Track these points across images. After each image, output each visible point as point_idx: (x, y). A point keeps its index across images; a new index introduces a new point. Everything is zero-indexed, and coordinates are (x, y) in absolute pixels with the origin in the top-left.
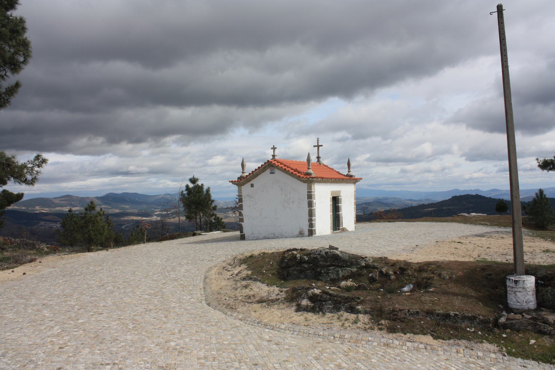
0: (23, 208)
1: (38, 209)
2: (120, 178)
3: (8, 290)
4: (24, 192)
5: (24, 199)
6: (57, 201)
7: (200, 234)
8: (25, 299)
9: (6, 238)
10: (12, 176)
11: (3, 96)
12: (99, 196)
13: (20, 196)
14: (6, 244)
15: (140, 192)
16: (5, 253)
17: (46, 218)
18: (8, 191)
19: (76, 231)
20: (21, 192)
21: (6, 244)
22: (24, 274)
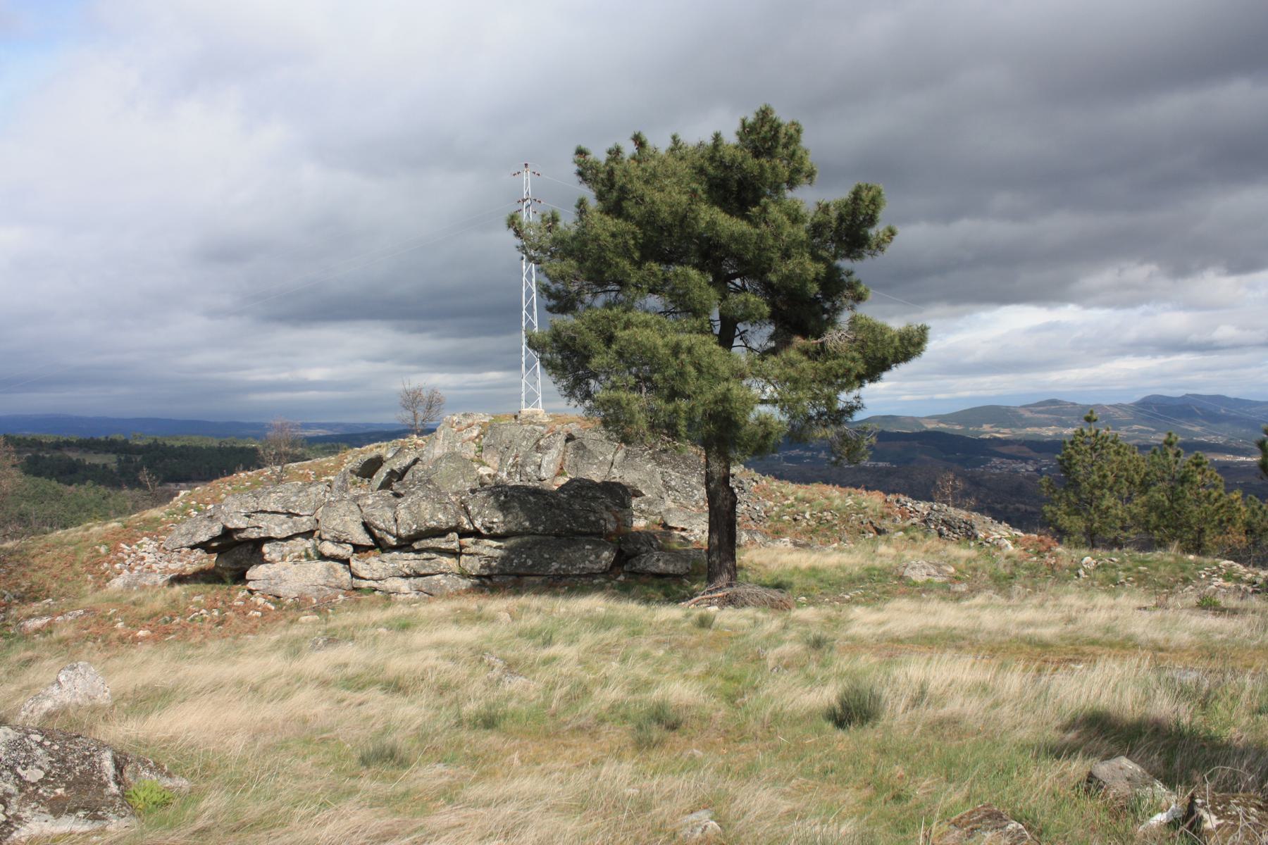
0: (957, 427)
1: (988, 431)
2: (1184, 359)
6: (1028, 414)
9: (891, 497)
12: (1126, 402)
14: (889, 515)
15: (1232, 392)
16: (883, 549)
17: (1004, 450)
19: (1111, 489)
21: (889, 515)
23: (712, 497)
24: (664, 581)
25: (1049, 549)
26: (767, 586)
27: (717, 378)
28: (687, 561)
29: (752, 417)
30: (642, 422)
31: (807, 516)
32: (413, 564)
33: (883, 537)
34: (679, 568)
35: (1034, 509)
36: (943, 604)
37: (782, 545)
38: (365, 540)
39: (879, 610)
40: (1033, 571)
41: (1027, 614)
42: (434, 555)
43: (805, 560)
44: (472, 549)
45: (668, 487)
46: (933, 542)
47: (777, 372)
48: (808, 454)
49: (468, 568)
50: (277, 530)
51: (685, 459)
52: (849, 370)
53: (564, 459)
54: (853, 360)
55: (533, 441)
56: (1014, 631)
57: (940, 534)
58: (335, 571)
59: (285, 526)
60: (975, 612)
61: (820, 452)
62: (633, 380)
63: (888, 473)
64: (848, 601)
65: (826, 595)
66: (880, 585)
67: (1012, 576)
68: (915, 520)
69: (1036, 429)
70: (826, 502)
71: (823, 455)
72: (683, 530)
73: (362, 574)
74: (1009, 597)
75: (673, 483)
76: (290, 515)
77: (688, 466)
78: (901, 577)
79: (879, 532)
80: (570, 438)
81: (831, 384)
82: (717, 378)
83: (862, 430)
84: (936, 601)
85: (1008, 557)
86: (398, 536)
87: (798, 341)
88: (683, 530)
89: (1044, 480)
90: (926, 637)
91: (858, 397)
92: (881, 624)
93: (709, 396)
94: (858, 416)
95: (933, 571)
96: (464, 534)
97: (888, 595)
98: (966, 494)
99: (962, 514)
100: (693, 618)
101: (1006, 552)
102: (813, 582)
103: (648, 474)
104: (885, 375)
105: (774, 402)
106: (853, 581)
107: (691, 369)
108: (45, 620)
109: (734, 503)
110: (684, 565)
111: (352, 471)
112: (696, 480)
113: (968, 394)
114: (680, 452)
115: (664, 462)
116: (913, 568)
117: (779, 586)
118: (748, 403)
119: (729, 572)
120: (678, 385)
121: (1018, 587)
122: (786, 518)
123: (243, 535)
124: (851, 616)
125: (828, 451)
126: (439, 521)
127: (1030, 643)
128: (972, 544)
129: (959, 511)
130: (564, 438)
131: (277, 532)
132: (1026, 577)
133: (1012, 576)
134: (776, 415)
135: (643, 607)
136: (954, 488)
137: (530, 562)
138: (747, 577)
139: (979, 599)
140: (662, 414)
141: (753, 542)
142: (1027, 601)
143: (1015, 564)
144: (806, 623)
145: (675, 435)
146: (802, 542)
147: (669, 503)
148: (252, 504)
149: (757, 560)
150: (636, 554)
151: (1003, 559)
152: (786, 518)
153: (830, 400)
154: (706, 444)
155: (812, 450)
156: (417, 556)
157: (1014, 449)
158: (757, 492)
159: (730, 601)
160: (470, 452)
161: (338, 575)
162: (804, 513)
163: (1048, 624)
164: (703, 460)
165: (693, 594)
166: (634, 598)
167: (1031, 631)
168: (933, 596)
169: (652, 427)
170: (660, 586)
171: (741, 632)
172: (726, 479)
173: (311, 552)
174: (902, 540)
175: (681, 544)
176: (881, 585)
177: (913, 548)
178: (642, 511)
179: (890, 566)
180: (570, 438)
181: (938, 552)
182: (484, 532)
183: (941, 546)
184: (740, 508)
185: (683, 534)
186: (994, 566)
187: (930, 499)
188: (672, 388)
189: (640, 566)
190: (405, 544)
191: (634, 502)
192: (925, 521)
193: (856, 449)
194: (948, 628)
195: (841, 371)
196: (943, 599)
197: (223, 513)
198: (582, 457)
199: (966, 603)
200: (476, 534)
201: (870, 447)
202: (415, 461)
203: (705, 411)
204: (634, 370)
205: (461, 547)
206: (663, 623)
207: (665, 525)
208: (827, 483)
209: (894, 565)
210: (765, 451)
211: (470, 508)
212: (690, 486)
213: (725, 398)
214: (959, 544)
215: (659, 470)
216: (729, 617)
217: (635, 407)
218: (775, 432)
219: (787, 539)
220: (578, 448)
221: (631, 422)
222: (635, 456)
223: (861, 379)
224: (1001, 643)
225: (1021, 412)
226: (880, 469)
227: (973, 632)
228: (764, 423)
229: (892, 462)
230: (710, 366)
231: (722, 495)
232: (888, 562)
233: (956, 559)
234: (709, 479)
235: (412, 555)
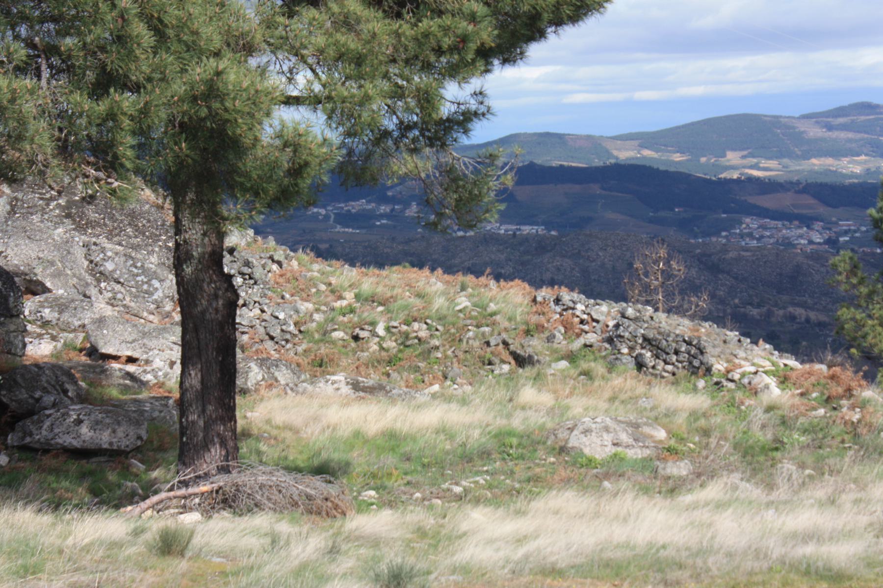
0: (677, 157)
1: (736, 164)
6: (815, 132)
9: (544, 293)
14: (540, 328)
16: (528, 394)
17: (767, 202)
21: (540, 328)
23: (186, 296)
24: (90, 465)
25: (849, 392)
26: (298, 470)
27: (194, 49)
28: (138, 423)
29: (267, 132)
30: (42, 138)
31: (380, 330)
34: (118, 436)
35: (823, 318)
36: (643, 500)
37: (330, 389)
39: (520, 513)
40: (818, 434)
41: (805, 518)
43: (374, 417)
45: (99, 275)
46: (626, 380)
47: (320, 40)
48: (384, 209)
51: (133, 216)
52: (464, 39)
54: (473, 18)
56: (777, 551)
57: (640, 365)
60: (703, 515)
61: (407, 204)
62: (21, 53)
63: (541, 246)
64: (459, 498)
65: (415, 485)
66: (522, 465)
67: (778, 445)
68: (591, 338)
69: (829, 161)
71: (413, 210)
72: (131, 360)
74: (771, 486)
75: (109, 266)
77: (140, 232)
78: (563, 450)
79: (521, 361)
81: (427, 67)
82: (194, 49)
83: (487, 157)
84: (629, 496)
85: (769, 409)
88: (131, 360)
89: (842, 260)
90: (607, 565)
91: (479, 94)
92: (520, 540)
93: (179, 88)
94: (481, 133)
95: (624, 437)
97: (537, 483)
98: (690, 288)
99: (683, 326)
100: (148, 536)
101: (765, 399)
102: (390, 460)
103: (57, 247)
104: (534, 50)
105: (313, 101)
106: (468, 458)
107: (139, 29)
109: (232, 305)
110: (132, 431)
112: (156, 258)
113: (698, 91)
114: (123, 199)
115: (90, 224)
116: (587, 432)
117: (324, 470)
118: (260, 103)
119: (223, 443)
120: (112, 60)
121: (788, 466)
122: (338, 335)
123: (745, 153)
124: (464, 526)
125: (410, 201)
127: (807, 573)
128: (701, 383)
129: (675, 319)
132: (802, 448)
133: (778, 445)
134: (316, 126)
135: (47, 519)
136: (667, 275)
138: (259, 453)
139: (713, 491)
140: (83, 121)
141: (272, 383)
142: (803, 494)
143: (784, 422)
144: (375, 542)
145: (111, 164)
146: (370, 382)
147: (101, 307)
149: (280, 419)
151: (759, 412)
152: (338, 335)
153: (427, 100)
154: (172, 183)
155: (392, 200)
157: (784, 201)
158: (282, 284)
159: (226, 501)
162: (373, 324)
163: (848, 534)
164: (170, 219)
165: (150, 489)
166: (28, 500)
167: (809, 549)
168: (624, 484)
169: (64, 150)
170: (82, 476)
171: (244, 562)
172: (215, 259)
174: (564, 377)
175: (125, 389)
176: (522, 464)
177: (588, 393)
178: (45, 324)
179: (542, 427)
181: (635, 399)
183: (641, 389)
184: (245, 316)
185: (131, 368)
186: (742, 426)
187: (621, 297)
188: (103, 67)
189: (42, 434)
191: (29, 305)
192: (610, 340)
193: (475, 198)
194: (650, 545)
195: (447, 42)
196: (645, 490)
199: (688, 498)
201: (504, 195)
203: (171, 121)
204: (23, 30)
206: (87, 549)
207: (93, 352)
208: (421, 267)
209: (550, 425)
210: (290, 199)
212: (145, 271)
213: (212, 91)
214: (676, 383)
215: (80, 238)
216: (224, 533)
217: (29, 107)
218: (314, 162)
219: (340, 377)
221: (20, 138)
222: (31, 210)
223: (486, 56)
224: (751, 574)
225: (802, 126)
226: (526, 239)
227: (702, 552)
228: (292, 143)
229: (549, 225)
230: (182, 26)
231: (209, 288)
232: (537, 419)
233: (670, 414)
234: (180, 257)
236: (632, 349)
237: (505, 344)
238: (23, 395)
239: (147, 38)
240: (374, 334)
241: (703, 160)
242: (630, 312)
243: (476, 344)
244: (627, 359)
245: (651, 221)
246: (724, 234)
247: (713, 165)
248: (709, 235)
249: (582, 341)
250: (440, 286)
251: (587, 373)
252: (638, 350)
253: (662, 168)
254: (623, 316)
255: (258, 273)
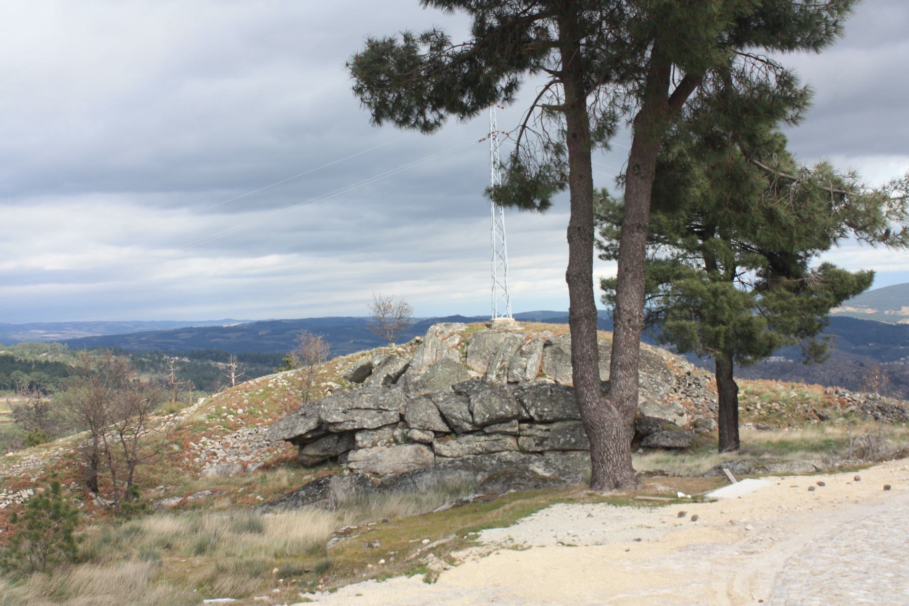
0: (869, 311)
3: (849, 527)
4: (874, 269)
5: (875, 286)
7: (308, 600)
8: (893, 556)
9: (829, 389)
10: (850, 225)
11: (825, 14)
13: (864, 280)
14: (830, 404)
16: (829, 430)
18: (832, 267)
20: (867, 269)
21: (830, 404)
22: (887, 488)
31: (759, 406)
32: (484, 444)
33: (826, 422)
38: (443, 427)
42: (501, 437)
44: (529, 432)
49: (526, 446)
50: (370, 422)
53: (542, 363)
54: (827, 296)
55: (516, 347)
57: (876, 418)
58: (422, 452)
59: (376, 419)
68: (853, 408)
70: (774, 394)
73: (445, 453)
76: (380, 410)
77: (652, 366)
79: (822, 418)
80: (547, 344)
86: (473, 423)
87: (784, 280)
96: (522, 421)
99: (894, 402)
108: (178, 500)
110: (687, 440)
111: (345, 377)
123: (340, 427)
126: (506, 411)
129: (890, 399)
130: (542, 344)
131: (369, 423)
137: (573, 440)
148: (348, 403)
150: (648, 434)
156: (487, 438)
160: (456, 356)
161: (425, 455)
162: (755, 404)
173: (400, 439)
180: (547, 344)
182: (536, 418)
189: (654, 441)
190: (479, 429)
197: (324, 410)
198: (560, 360)
200: (531, 421)
202: (407, 367)
205: (520, 430)
211: (525, 401)
212: (656, 383)
220: (556, 353)
235: (483, 438)
236: (872, 412)
237: (815, 411)
238: (644, 427)
239: (728, 307)
240: (756, 408)
241: (886, 312)
242: (870, 396)
243: (802, 411)
244: (870, 416)
245: (853, 352)
246: (902, 359)
247: (894, 316)
248: (893, 360)
249: (849, 409)
250: (782, 387)
251: (853, 422)
252: (875, 412)
253: (860, 318)
254: (868, 398)
255: (702, 383)
